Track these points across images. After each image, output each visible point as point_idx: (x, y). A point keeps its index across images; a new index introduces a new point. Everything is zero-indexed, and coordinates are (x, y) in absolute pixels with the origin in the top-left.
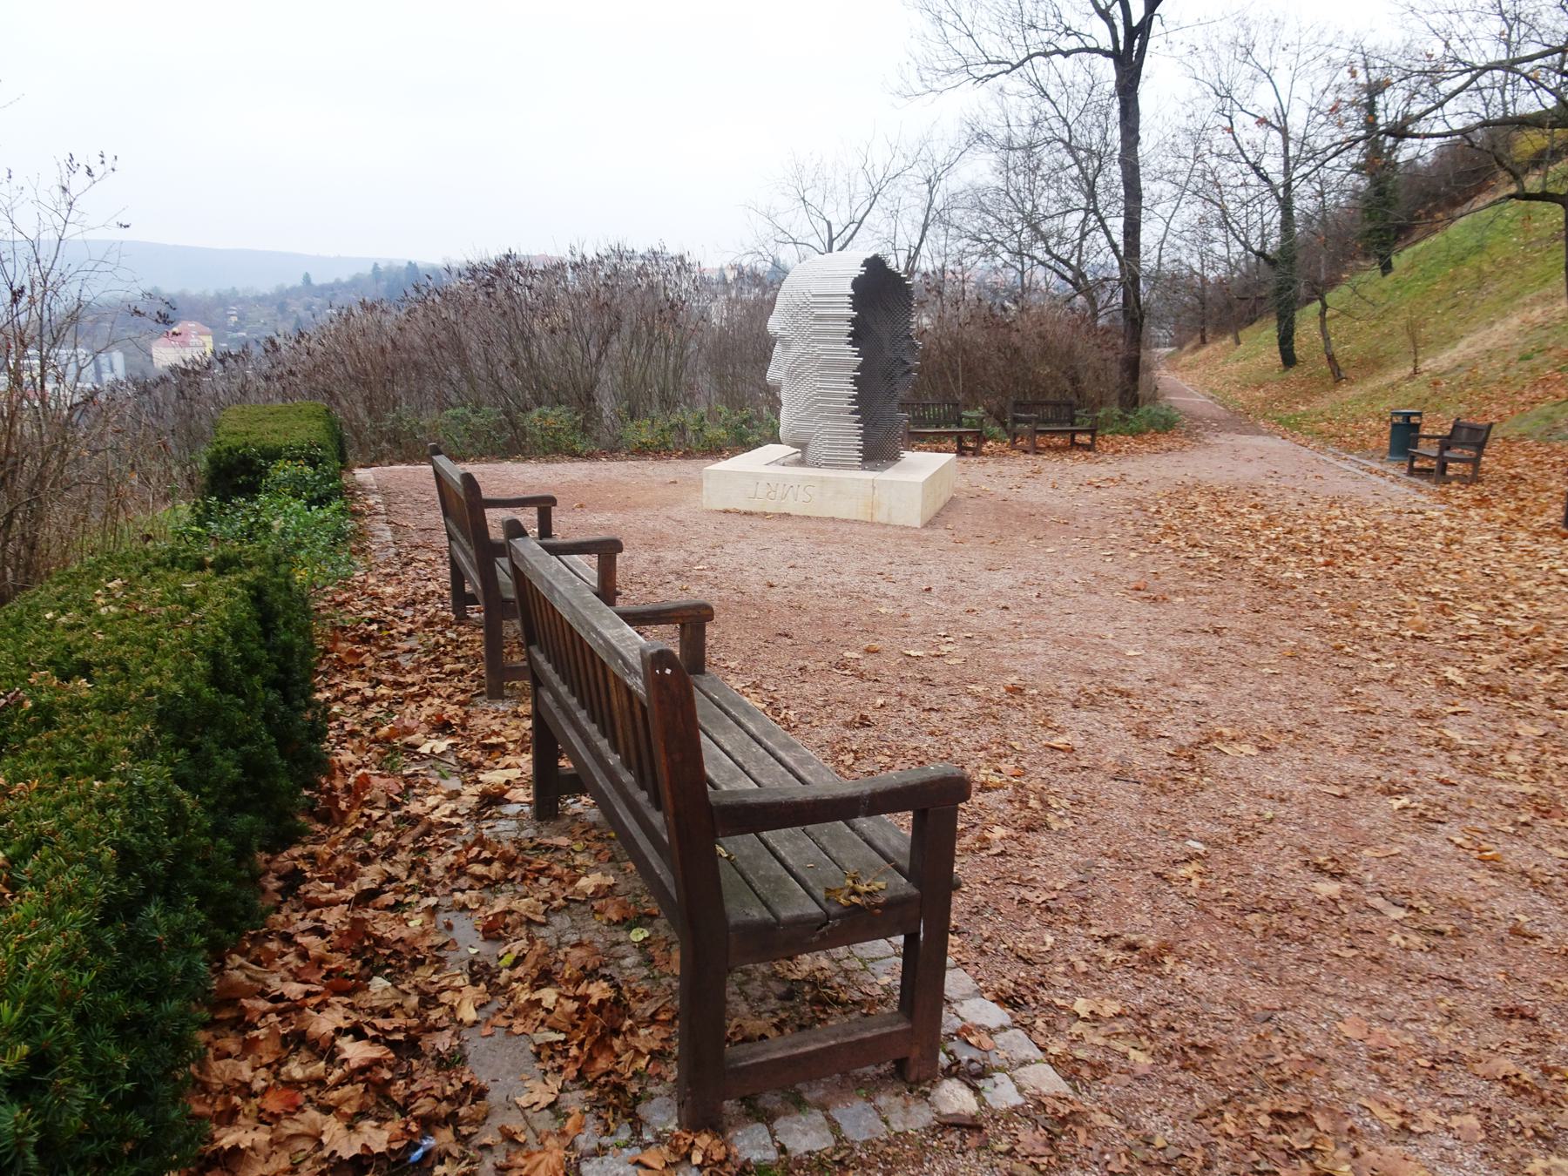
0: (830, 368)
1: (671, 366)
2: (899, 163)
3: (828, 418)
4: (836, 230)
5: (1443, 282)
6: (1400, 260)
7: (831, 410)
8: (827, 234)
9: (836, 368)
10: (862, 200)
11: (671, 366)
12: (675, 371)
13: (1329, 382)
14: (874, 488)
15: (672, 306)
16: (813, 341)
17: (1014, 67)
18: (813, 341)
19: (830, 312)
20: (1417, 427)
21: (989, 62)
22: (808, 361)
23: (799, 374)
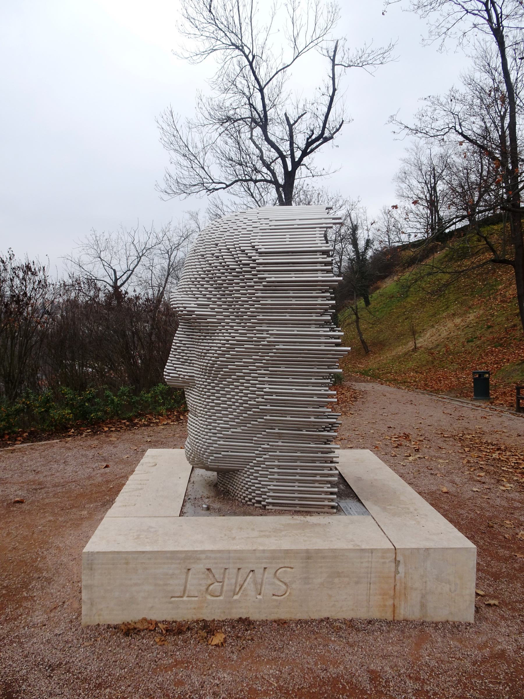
0: (288, 363)
1: (16, 353)
2: (152, 241)
3: (280, 436)
4: (119, 274)
5: (396, 309)
6: (374, 296)
7: (286, 426)
8: (113, 276)
9: (299, 363)
10: (133, 258)
11: (16, 353)
12: (20, 357)
13: (363, 352)
14: (397, 563)
15: (18, 302)
16: (261, 322)
17: (227, 186)
18: (261, 322)
19: (293, 277)
20: (487, 379)
21: (214, 182)
22: (249, 353)
23: (232, 372)
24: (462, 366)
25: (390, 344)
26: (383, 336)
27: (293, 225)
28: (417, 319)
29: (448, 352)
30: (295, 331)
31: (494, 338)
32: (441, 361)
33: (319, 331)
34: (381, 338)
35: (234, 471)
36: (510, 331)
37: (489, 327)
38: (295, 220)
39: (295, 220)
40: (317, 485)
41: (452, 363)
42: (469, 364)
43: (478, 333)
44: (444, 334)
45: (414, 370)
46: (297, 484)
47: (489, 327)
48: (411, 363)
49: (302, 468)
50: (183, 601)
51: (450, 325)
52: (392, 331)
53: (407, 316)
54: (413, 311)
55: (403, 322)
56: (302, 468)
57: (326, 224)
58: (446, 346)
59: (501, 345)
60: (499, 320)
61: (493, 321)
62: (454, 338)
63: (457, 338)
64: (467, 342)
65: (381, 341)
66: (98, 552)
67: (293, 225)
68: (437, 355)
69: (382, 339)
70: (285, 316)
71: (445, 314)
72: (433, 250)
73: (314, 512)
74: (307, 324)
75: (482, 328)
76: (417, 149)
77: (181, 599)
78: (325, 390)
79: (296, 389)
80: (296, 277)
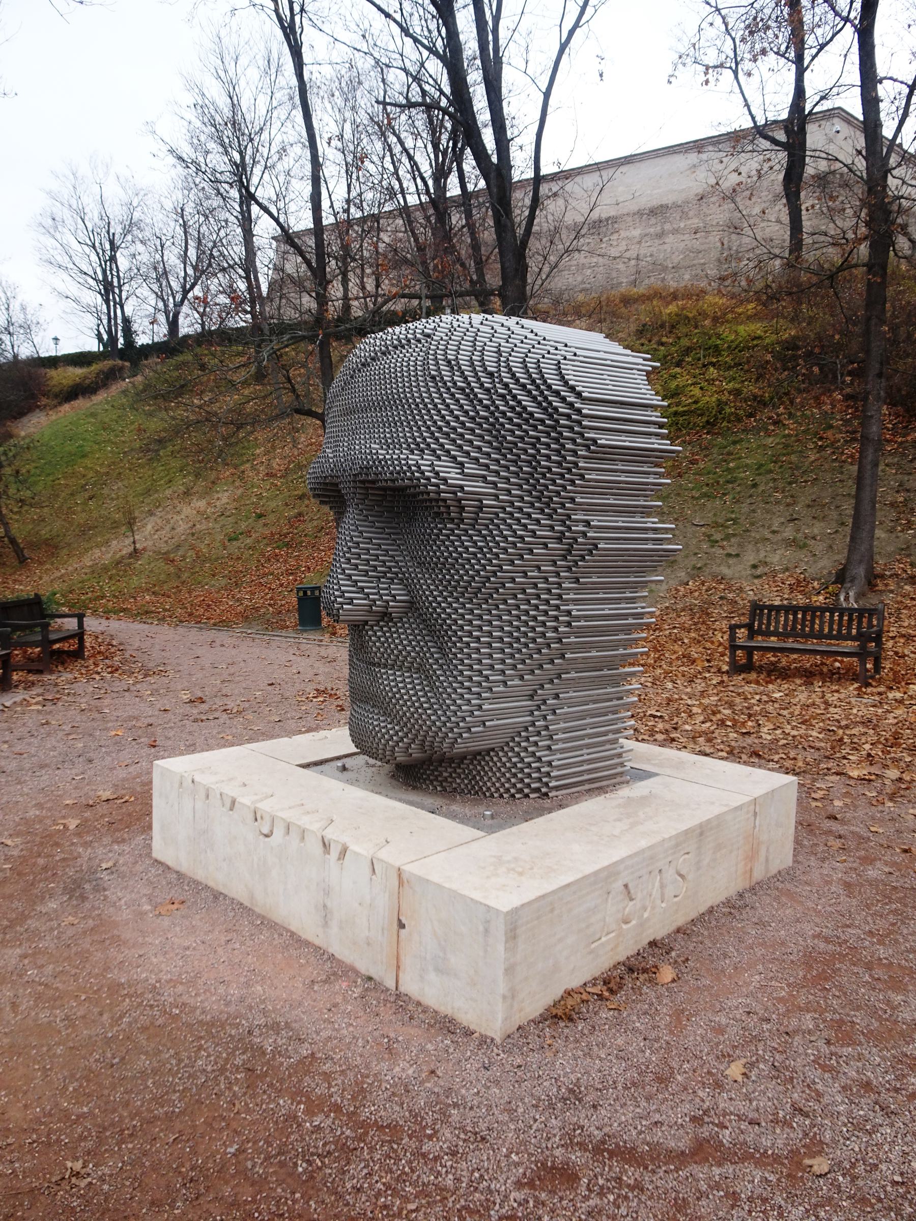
5: (65, 478)
24: (234, 580)
25: (69, 545)
26: (48, 528)
27: (606, 360)
28: (112, 499)
29: (200, 558)
30: (620, 521)
31: (272, 534)
32: (193, 574)
33: (646, 523)
34: (44, 532)
35: (477, 755)
36: (294, 522)
37: (260, 516)
38: (599, 351)
39: (599, 351)
40: (608, 747)
41: (214, 576)
42: (244, 576)
43: (243, 526)
44: (182, 527)
45: (148, 590)
46: (585, 751)
47: (260, 516)
48: (135, 578)
49: (594, 726)
50: (602, 944)
51: (187, 511)
52: (65, 520)
53: (91, 493)
54: (102, 485)
55: (85, 503)
56: (594, 726)
57: (612, 361)
58: (192, 547)
59: (287, 545)
60: (273, 504)
61: (263, 506)
62: (204, 534)
63: (210, 534)
64: (229, 540)
65: (47, 539)
66: (523, 905)
67: (606, 360)
68: (182, 563)
69: (48, 536)
70: (608, 499)
71: (168, 492)
72: (109, 377)
73: (608, 786)
74: (646, 512)
75: (248, 518)
76: (76, 178)
77: (600, 942)
78: (643, 608)
79: (610, 609)
80: (630, 442)
